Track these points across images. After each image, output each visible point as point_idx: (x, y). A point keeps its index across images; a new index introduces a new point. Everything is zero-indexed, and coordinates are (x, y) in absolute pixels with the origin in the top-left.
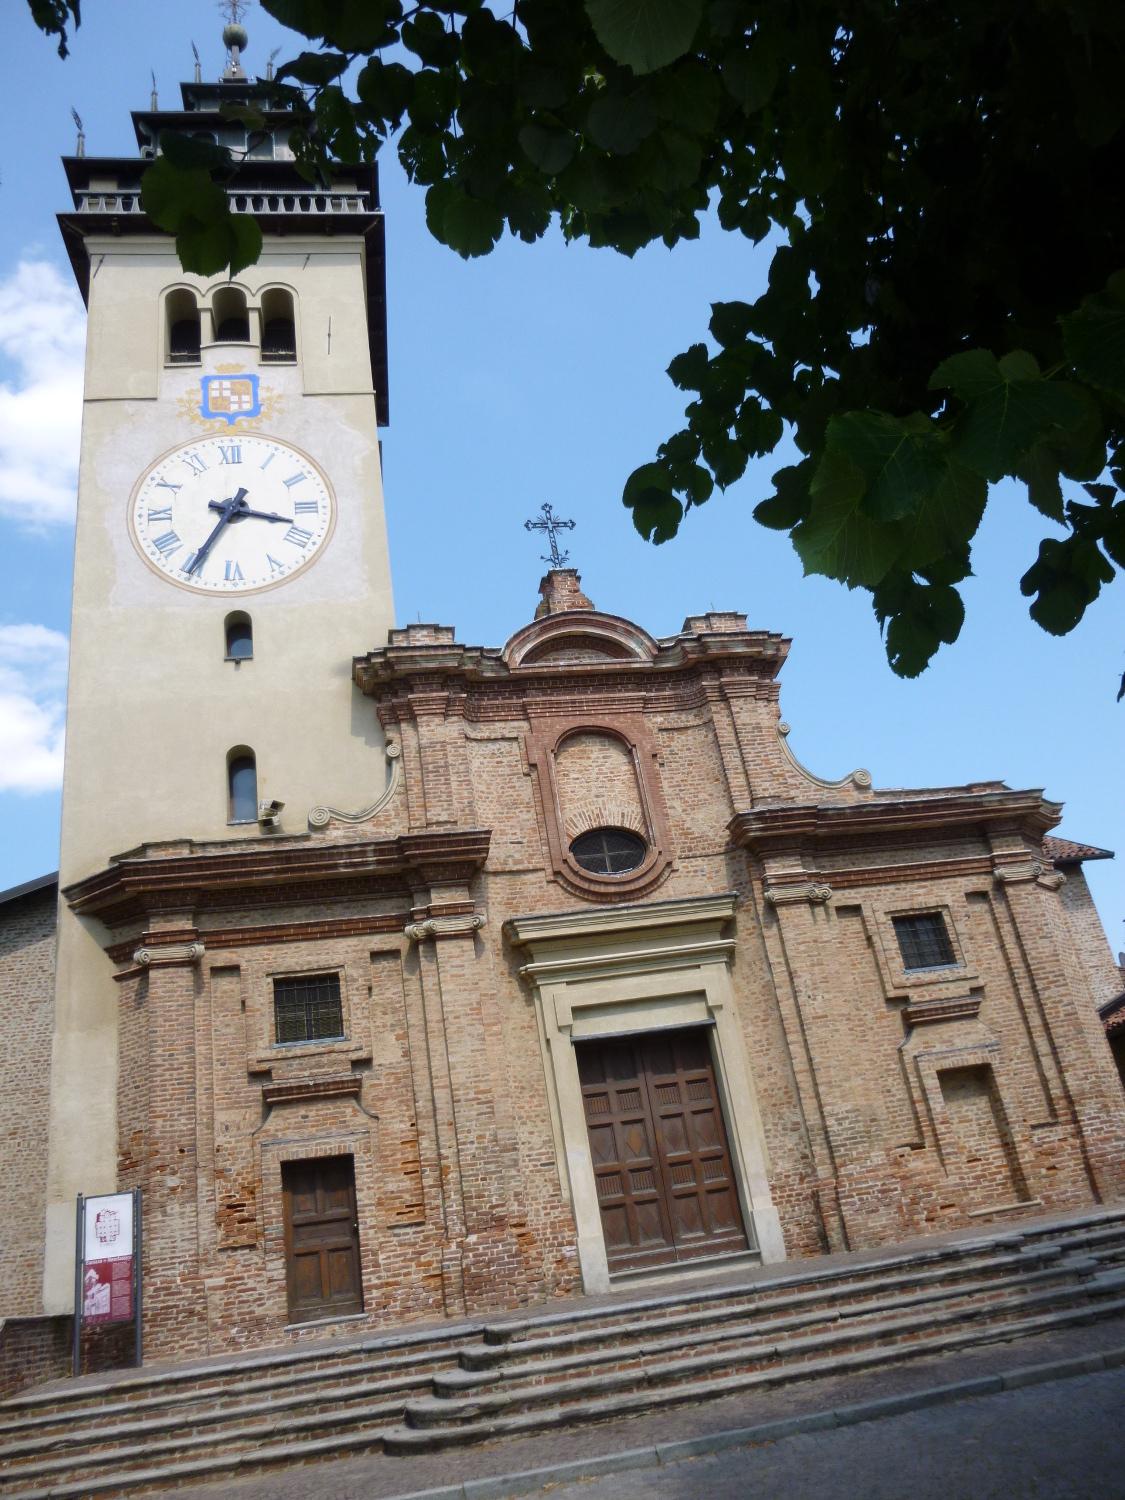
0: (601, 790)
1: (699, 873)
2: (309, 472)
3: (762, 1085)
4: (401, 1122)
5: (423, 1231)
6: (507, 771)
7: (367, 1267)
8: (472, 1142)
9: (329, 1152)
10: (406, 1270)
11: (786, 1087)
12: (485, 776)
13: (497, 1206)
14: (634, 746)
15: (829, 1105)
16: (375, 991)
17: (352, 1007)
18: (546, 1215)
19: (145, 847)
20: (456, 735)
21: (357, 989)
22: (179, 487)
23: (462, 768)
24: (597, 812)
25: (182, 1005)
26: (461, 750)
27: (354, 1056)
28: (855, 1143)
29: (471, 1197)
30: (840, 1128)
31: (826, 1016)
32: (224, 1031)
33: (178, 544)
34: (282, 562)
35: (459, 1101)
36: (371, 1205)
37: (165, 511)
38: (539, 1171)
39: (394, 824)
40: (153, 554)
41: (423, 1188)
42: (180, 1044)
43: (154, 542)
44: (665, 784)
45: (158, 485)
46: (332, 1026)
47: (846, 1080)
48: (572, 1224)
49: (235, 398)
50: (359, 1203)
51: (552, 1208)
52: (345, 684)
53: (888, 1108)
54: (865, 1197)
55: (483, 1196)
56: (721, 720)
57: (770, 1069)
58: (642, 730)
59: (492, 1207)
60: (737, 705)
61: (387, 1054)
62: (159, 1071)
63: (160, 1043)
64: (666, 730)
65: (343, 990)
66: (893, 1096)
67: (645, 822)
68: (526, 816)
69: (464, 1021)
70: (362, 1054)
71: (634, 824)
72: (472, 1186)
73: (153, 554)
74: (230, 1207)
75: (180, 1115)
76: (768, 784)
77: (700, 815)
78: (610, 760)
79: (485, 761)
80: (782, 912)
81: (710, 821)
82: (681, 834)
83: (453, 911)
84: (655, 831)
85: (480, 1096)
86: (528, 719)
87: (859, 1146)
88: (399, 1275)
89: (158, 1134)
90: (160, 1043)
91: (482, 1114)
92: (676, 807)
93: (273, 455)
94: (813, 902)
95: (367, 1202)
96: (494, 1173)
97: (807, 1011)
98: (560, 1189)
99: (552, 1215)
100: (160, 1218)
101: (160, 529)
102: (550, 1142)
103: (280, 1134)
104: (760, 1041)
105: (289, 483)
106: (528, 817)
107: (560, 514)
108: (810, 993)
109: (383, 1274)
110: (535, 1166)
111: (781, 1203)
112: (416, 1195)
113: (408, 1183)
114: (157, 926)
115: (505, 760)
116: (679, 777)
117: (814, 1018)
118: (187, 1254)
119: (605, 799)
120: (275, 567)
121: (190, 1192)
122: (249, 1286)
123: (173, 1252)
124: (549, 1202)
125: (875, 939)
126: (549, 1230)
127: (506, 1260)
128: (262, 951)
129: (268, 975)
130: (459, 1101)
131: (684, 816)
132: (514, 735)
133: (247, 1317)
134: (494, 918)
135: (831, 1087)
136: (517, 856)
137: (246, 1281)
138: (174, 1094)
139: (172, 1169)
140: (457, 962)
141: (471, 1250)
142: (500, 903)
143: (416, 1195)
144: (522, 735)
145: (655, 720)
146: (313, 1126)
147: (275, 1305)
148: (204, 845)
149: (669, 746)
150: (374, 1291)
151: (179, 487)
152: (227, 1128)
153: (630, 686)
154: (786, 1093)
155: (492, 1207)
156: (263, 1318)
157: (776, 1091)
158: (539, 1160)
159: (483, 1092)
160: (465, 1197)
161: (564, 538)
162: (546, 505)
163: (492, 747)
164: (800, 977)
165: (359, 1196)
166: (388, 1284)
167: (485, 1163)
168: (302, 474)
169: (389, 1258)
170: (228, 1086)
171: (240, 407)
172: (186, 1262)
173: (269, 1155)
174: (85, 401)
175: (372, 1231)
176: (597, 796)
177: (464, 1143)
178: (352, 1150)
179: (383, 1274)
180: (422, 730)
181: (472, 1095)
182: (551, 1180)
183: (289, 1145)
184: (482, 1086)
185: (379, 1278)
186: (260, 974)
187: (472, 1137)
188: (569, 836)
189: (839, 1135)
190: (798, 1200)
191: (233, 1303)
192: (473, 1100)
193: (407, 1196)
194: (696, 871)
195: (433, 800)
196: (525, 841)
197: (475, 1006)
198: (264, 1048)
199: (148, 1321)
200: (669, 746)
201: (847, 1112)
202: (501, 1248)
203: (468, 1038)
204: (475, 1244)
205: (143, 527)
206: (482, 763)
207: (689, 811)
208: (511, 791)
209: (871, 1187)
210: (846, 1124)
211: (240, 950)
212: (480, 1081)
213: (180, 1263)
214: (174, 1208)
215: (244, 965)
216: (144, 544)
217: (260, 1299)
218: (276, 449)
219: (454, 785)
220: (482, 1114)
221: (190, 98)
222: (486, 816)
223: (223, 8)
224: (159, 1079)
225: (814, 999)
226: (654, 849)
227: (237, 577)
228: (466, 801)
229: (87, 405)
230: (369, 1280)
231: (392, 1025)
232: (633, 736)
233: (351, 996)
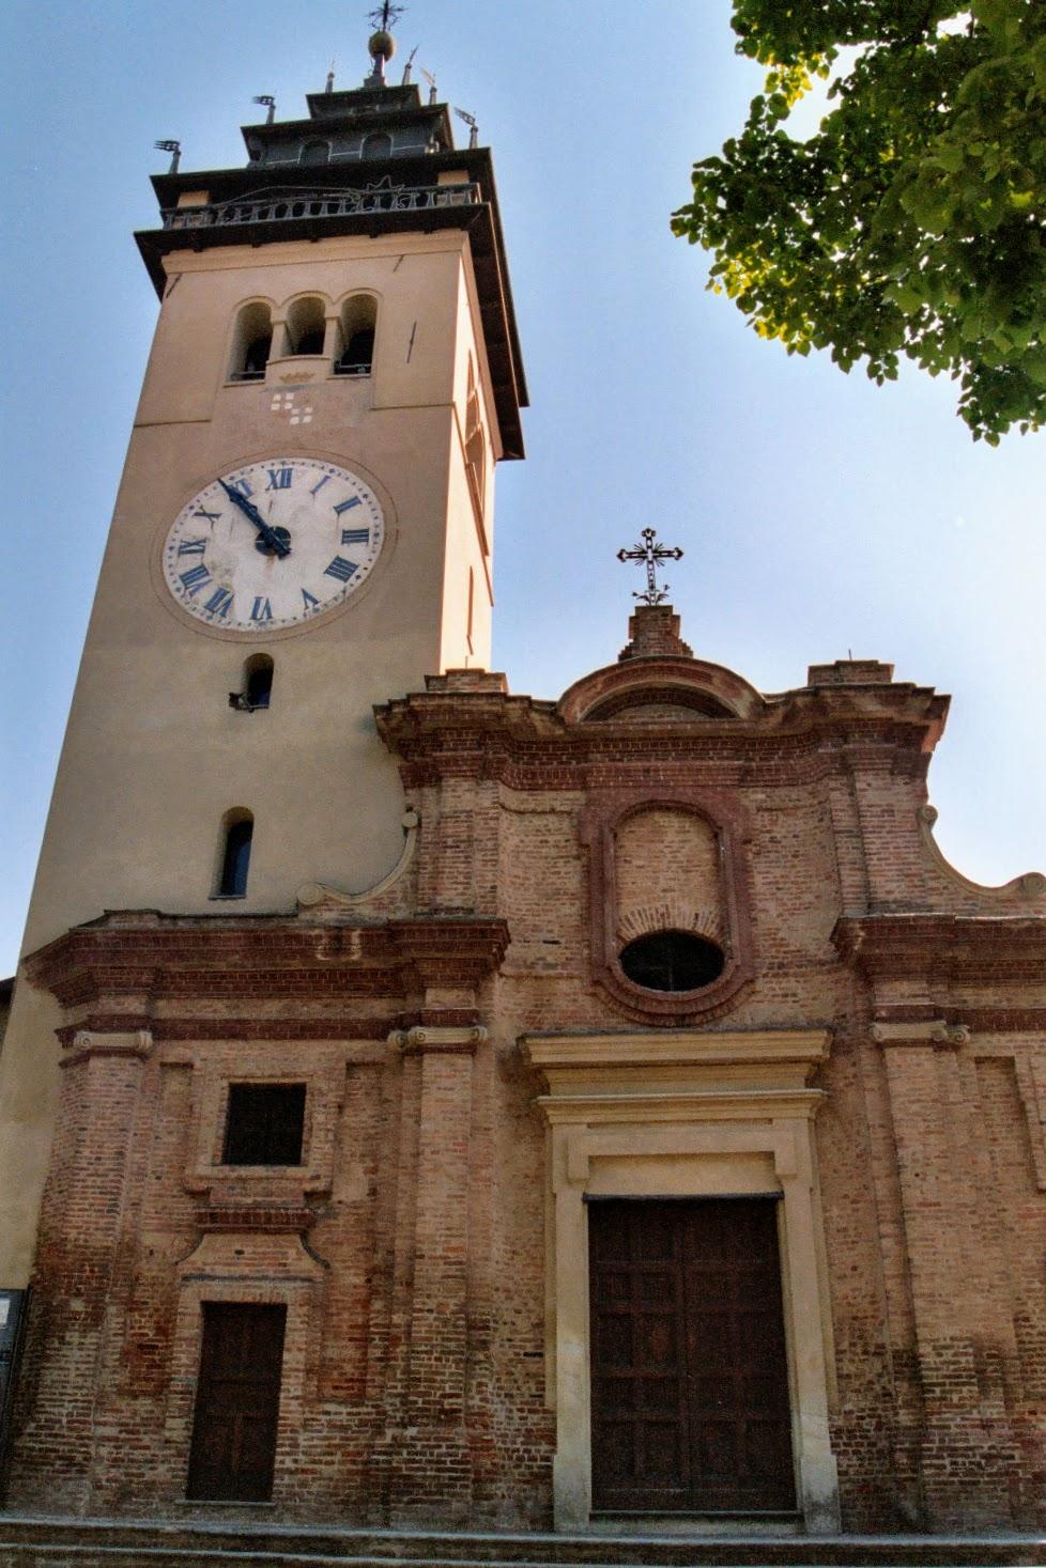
0: (672, 883)
1: (790, 999)
2: (365, 496)
3: (842, 1289)
4: (356, 1275)
5: (359, 1414)
6: (553, 852)
7: (282, 1445)
8: (430, 1311)
9: (258, 1299)
10: (329, 1458)
11: (873, 1296)
12: (523, 857)
13: (451, 1396)
14: (721, 828)
15: (925, 1325)
16: (348, 1111)
17: (315, 1127)
18: (521, 1418)
19: (109, 914)
20: (487, 803)
21: (325, 1106)
22: (217, 516)
23: (490, 844)
24: (663, 910)
25: (118, 1103)
26: (492, 823)
27: (308, 1187)
28: (957, 1384)
29: (419, 1380)
30: (938, 1360)
31: (938, 1204)
32: (165, 1140)
33: (206, 579)
34: (317, 598)
35: (422, 1257)
36: (297, 1370)
37: (197, 544)
38: (521, 1361)
39: (398, 908)
40: (178, 590)
41: (367, 1361)
42: (110, 1149)
43: (181, 577)
44: (758, 879)
45: (197, 514)
46: (291, 1153)
47: (956, 1295)
48: (550, 1437)
49: (289, 406)
50: (285, 1366)
51: (530, 1411)
52: (369, 738)
53: (1021, 1342)
54: (960, 1460)
55: (435, 1381)
56: (839, 799)
57: (854, 1268)
58: (735, 807)
59: (444, 1396)
60: (863, 781)
61: (351, 1190)
62: (82, 1175)
63: (88, 1143)
64: (767, 810)
65: (308, 1104)
66: (1032, 1327)
67: (724, 928)
68: (567, 910)
69: (444, 1158)
70: (320, 1185)
71: (707, 929)
72: (421, 1366)
73: (178, 590)
74: (141, 1346)
75: (97, 1229)
76: (895, 885)
77: (800, 922)
78: (687, 846)
79: (526, 839)
80: (892, 1054)
81: (809, 933)
82: (772, 946)
83: (450, 1019)
84: (734, 941)
85: (450, 1254)
86: (585, 787)
87: (965, 1389)
88: (320, 1462)
89: (69, 1247)
90: (88, 1143)
91: (449, 1277)
92: (769, 911)
93: (327, 478)
94: (939, 1046)
95: (295, 1366)
96: (450, 1353)
97: (912, 1196)
98: (544, 1389)
99: (530, 1421)
100: (56, 1345)
101: (190, 562)
102: (540, 1325)
103: (208, 1268)
104: (845, 1229)
105: (340, 509)
106: (570, 910)
107: (664, 541)
108: (918, 1170)
109: (301, 1457)
110: (517, 1354)
111: (845, 1453)
112: (358, 1368)
113: (351, 1352)
114: (109, 1005)
115: (550, 838)
116: (778, 872)
117: (921, 1204)
118: (79, 1392)
119: (675, 894)
120: (310, 604)
121: (96, 1317)
122: (142, 1444)
123: (64, 1387)
124: (527, 1403)
125: (1029, 1106)
126: (521, 1439)
127: (449, 1465)
128: (224, 1049)
129: (223, 1077)
130: (422, 1257)
131: (779, 921)
132: (567, 808)
133: (135, 1480)
134: (502, 1029)
135: (933, 1302)
136: (550, 959)
137: (141, 1436)
138: (92, 1205)
139: (78, 1289)
140: (447, 1083)
141: (407, 1446)
142: (519, 1016)
143: (358, 1368)
144: (576, 809)
145: (753, 797)
146: (247, 1265)
147: (168, 1471)
148: (175, 918)
149: (769, 832)
150: (286, 1477)
151: (217, 516)
152: (151, 1252)
153: (725, 753)
154: (873, 1303)
155: (444, 1396)
156: (154, 1482)
157: (859, 1299)
158: (521, 1347)
159: (454, 1250)
160: (412, 1380)
161: (666, 572)
162: (648, 530)
163: (537, 822)
164: (907, 1147)
165: (286, 1356)
166: (304, 1471)
167: (443, 1339)
168: (356, 498)
169: (312, 1439)
170: (160, 1205)
171: (301, 420)
172: (76, 1401)
173: (189, 1290)
174: (136, 426)
175: (294, 1402)
176: (664, 891)
177: (421, 1311)
178: (288, 1300)
179: (301, 1457)
180: (447, 795)
181: (439, 1253)
182: (535, 1375)
183: (213, 1283)
184: (454, 1243)
185: (296, 1461)
186: (215, 1076)
187: (432, 1304)
188: (619, 937)
189: (937, 1369)
190: (869, 1452)
191: (123, 1461)
192: (441, 1257)
193: (348, 1368)
194: (786, 996)
195: (446, 881)
196: (563, 940)
197: (460, 1140)
198: (205, 1165)
199: (22, 1462)
200: (769, 832)
201: (952, 1339)
202: (405, 1456)
203: (445, 1179)
204: (412, 1438)
205: (173, 561)
206: (522, 841)
207: (786, 916)
208: (554, 878)
209: (971, 1449)
210: (948, 1355)
211: (195, 1044)
212: (451, 1236)
213: (70, 1401)
214: (73, 1337)
215: (198, 1064)
216: (169, 580)
217: (151, 1462)
218: (332, 471)
219: (477, 865)
220: (449, 1277)
221: (317, 111)
222: (513, 903)
223: (373, 18)
224: (80, 1184)
225: (923, 1179)
226: (730, 965)
227: (265, 616)
228: (489, 885)
229: (139, 429)
230: (282, 1462)
231: (363, 1155)
232: (722, 814)
233: (318, 1116)
